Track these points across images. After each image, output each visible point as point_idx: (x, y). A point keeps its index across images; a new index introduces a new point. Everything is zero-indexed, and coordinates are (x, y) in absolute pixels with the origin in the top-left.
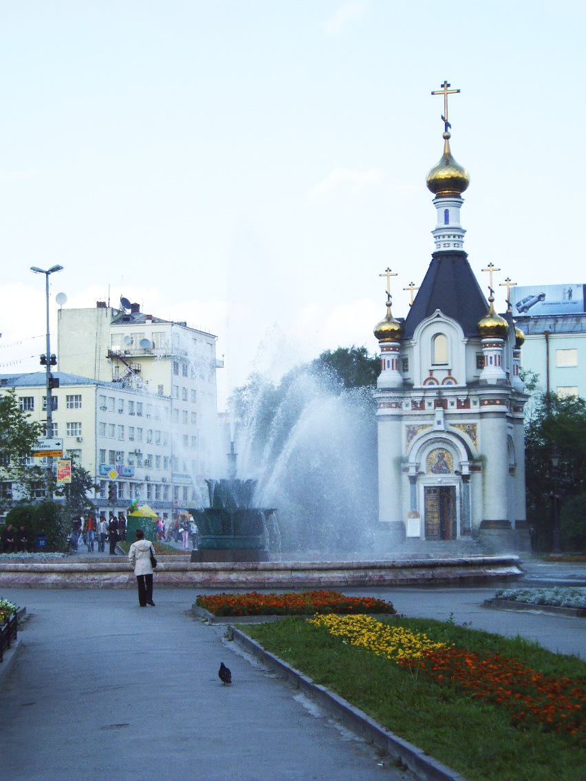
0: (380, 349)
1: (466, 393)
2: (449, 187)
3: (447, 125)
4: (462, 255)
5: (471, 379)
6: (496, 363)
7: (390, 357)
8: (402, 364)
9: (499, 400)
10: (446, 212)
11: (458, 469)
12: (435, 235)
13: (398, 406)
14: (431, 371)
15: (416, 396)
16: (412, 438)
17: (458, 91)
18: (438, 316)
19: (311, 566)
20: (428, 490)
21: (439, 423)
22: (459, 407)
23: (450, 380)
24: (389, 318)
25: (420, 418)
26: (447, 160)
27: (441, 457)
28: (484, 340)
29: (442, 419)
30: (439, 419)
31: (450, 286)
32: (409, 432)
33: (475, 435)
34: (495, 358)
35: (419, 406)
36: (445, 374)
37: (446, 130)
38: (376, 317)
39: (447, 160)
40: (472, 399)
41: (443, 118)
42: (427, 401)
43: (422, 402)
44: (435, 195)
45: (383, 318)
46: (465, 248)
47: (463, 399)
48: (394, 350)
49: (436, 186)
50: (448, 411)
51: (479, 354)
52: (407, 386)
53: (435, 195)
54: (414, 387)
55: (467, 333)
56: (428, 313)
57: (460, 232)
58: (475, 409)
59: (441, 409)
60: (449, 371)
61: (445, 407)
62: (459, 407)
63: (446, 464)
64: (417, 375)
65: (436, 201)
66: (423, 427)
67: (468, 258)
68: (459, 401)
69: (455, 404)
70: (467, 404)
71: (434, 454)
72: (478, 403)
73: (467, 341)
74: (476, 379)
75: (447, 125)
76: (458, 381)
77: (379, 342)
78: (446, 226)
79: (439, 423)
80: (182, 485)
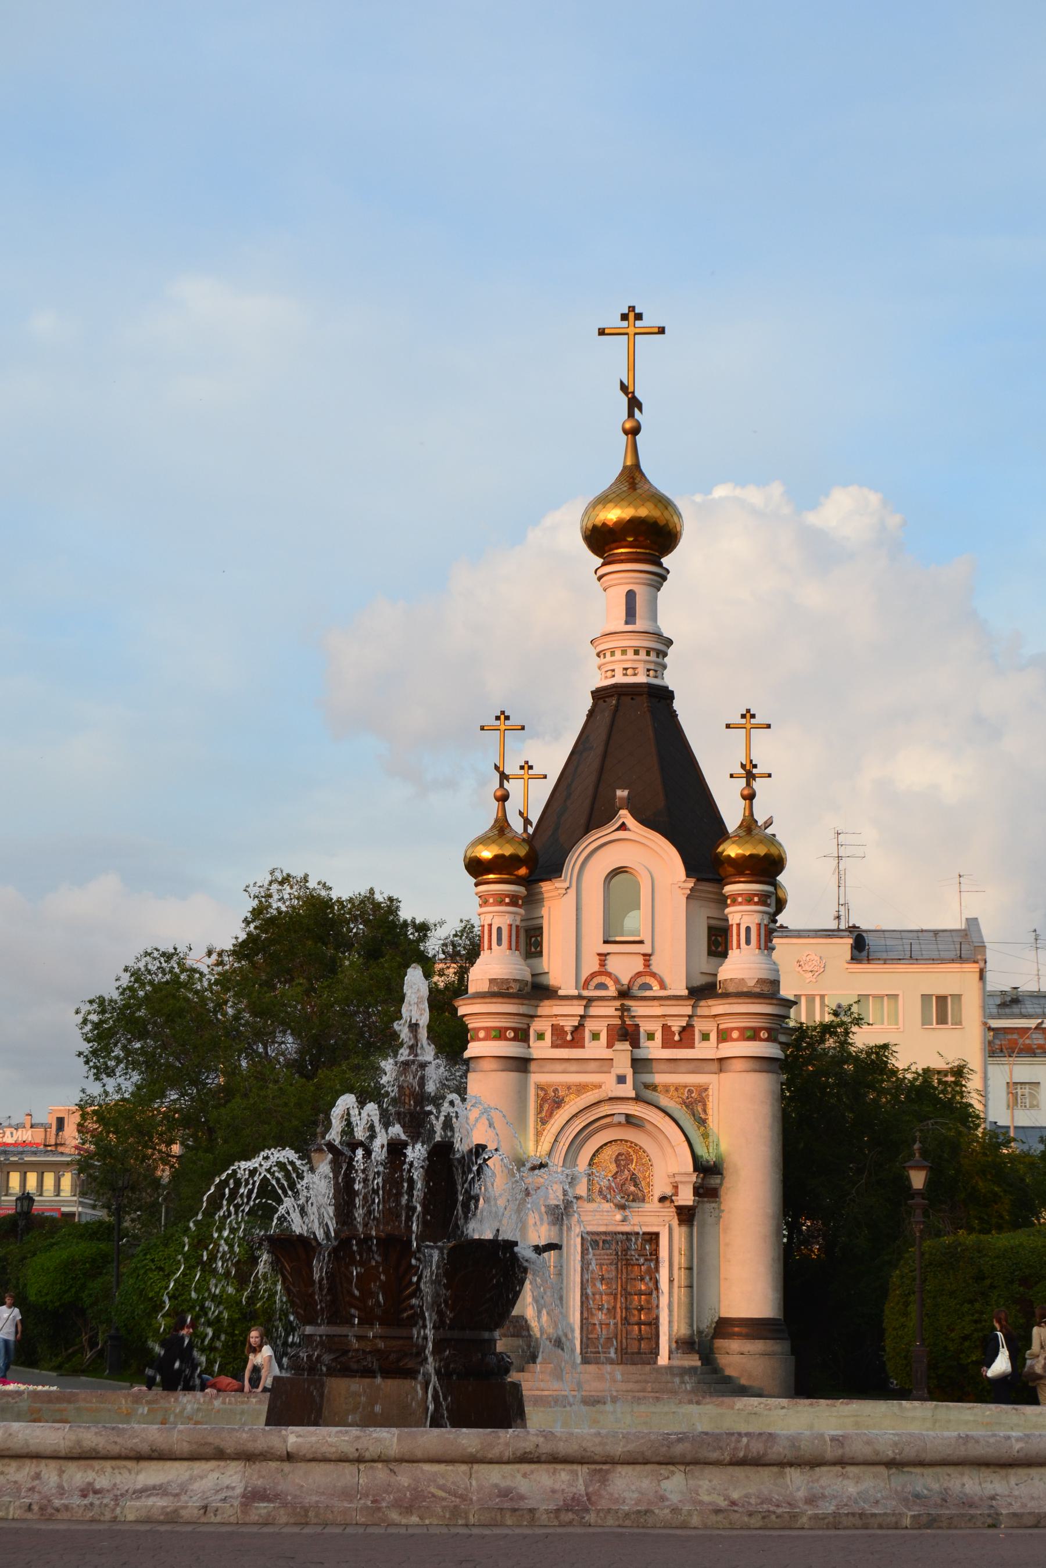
0: (478, 900)
1: (688, 1011)
2: (639, 537)
3: (634, 404)
4: (665, 696)
5: (700, 981)
6: (759, 941)
7: (501, 918)
8: (530, 940)
9: (737, 1029)
10: (631, 596)
11: (668, 1191)
12: (599, 649)
13: (522, 1036)
14: (603, 957)
15: (567, 1013)
16: (551, 1115)
17: (662, 331)
18: (623, 827)
19: (962, 1452)
20: (593, 1241)
21: (621, 1079)
22: (667, 1044)
23: (649, 980)
24: (501, 827)
25: (574, 1067)
26: (632, 478)
27: (622, 1161)
28: (729, 889)
29: (629, 1072)
30: (621, 1071)
31: (637, 756)
32: (542, 1101)
33: (705, 1111)
34: (759, 930)
35: (569, 1038)
36: (638, 965)
37: (631, 414)
38: (466, 818)
39: (632, 478)
40: (699, 1026)
41: (624, 388)
42: (590, 1026)
43: (578, 1029)
44: (601, 561)
45: (486, 822)
46: (670, 680)
47: (676, 1025)
48: (501, 903)
49: (601, 540)
50: (641, 1053)
51: (713, 922)
52: (538, 990)
53: (601, 561)
54: (561, 993)
55: (691, 869)
56: (599, 815)
57: (660, 646)
58: (703, 1050)
59: (626, 1046)
60: (647, 957)
61: (635, 1044)
62: (667, 1044)
63: (634, 1180)
64: (558, 966)
65: (600, 572)
66: (581, 1089)
67: (677, 705)
68: (666, 1028)
69: (658, 1035)
70: (686, 1036)
71: (609, 1153)
72: (713, 1036)
73: (692, 890)
74: (709, 979)
75: (634, 404)
76: (667, 981)
77: (477, 885)
78: (630, 628)
79: (621, 1079)
80: (950, 1026)
